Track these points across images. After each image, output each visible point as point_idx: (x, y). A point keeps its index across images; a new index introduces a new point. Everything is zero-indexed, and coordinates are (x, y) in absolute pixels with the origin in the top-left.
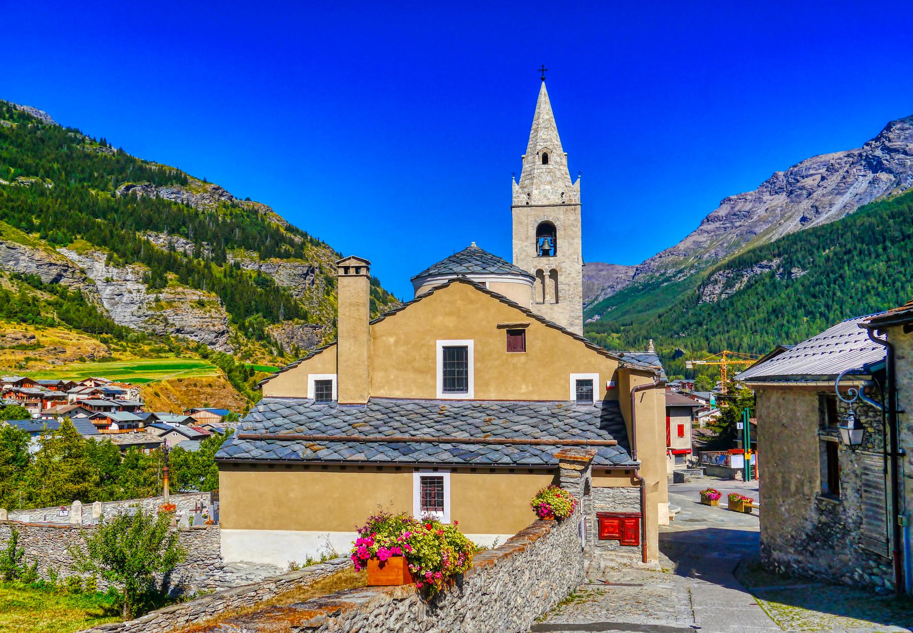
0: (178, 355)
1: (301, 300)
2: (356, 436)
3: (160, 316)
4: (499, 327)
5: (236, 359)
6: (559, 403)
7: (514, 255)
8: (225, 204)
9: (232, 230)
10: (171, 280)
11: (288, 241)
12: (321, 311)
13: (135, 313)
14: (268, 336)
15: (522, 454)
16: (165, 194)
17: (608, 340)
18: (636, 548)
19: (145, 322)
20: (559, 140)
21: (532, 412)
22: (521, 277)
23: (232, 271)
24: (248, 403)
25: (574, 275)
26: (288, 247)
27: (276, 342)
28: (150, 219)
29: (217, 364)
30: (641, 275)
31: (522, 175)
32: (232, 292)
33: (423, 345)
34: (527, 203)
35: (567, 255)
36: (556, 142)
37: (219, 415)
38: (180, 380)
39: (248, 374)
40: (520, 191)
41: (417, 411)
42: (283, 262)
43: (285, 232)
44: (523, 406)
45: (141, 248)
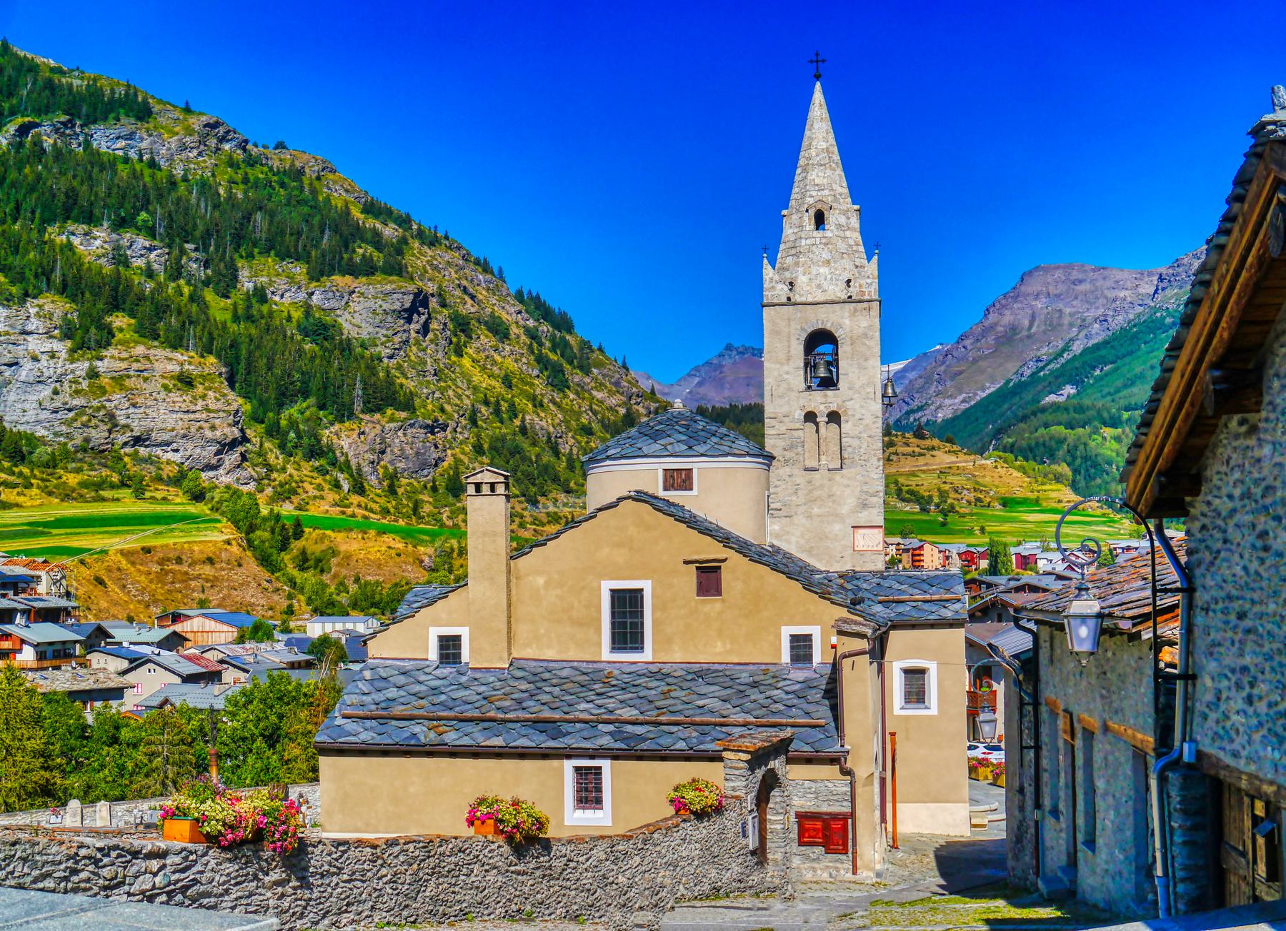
0: (139, 493)
1: (399, 367)
2: (492, 714)
3: (99, 409)
4: (686, 562)
5: (261, 499)
6: (765, 669)
7: (767, 389)
8: (231, 157)
9: (248, 217)
10: (121, 330)
11: (369, 235)
12: (443, 391)
13: (47, 404)
14: (331, 449)
15: (702, 738)
16: (105, 139)
17: (1093, 444)
18: (844, 857)
19: (69, 423)
20: (845, 184)
21: (728, 679)
22: (748, 459)
23: (249, 307)
24: (290, 597)
25: (868, 420)
26: (370, 249)
27: (347, 462)
28: (72, 195)
29: (223, 514)
30: (1169, 292)
31: (782, 247)
32: (250, 353)
33: (583, 588)
34: (789, 299)
35: (857, 386)
36: (840, 190)
37: (233, 626)
38: (147, 550)
39: (289, 533)
40: (776, 277)
41: (575, 679)
42: (360, 283)
43: (362, 216)
44: (717, 671)
45: (55, 261)
